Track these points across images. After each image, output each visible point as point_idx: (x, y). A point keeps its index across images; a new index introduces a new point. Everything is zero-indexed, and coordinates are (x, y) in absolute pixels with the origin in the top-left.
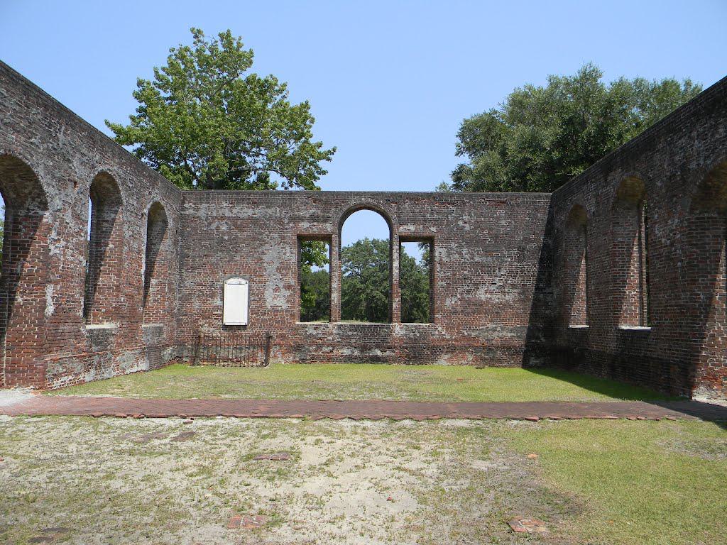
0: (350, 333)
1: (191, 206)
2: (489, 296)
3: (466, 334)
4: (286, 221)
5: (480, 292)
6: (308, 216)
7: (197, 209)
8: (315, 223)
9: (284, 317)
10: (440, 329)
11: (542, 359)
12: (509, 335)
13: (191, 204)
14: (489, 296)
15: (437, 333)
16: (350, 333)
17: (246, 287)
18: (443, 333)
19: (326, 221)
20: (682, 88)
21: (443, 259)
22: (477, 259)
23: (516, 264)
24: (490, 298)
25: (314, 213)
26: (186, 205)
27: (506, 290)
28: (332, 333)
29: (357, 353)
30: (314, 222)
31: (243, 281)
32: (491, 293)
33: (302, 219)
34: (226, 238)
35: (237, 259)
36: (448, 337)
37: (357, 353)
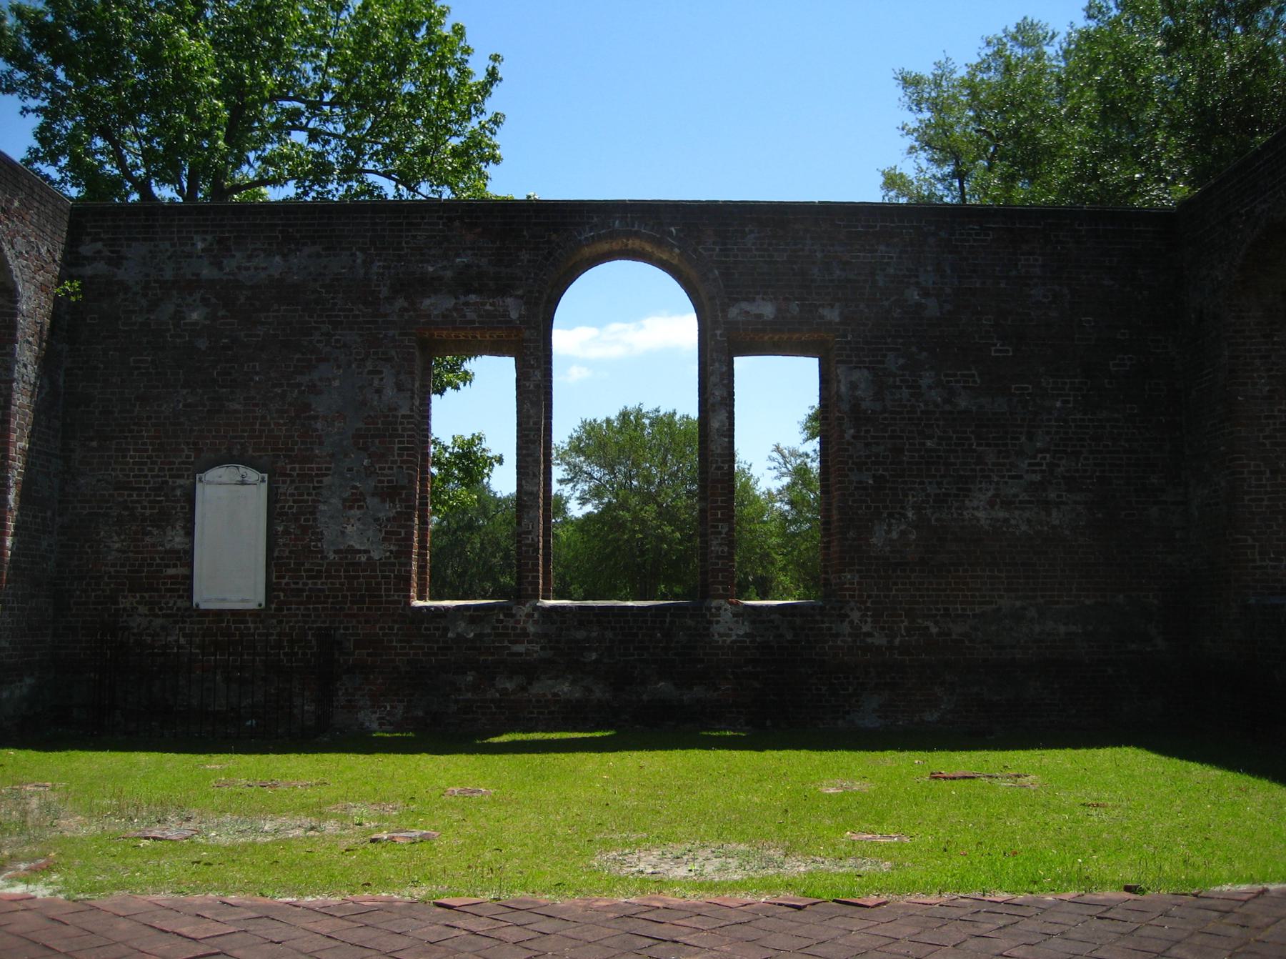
0: (581, 635)
1: (99, 252)
2: (1002, 514)
3: (934, 630)
4: (385, 292)
5: (975, 503)
6: (449, 274)
7: (117, 260)
8: (473, 298)
9: (378, 584)
10: (856, 616)
11: (129, 201)
12: (1062, 629)
13: (99, 245)
14: (1002, 514)
15: (846, 628)
16: (581, 635)
17: (196, 599)
18: (865, 629)
19: (503, 291)
20: (927, 115)
21: (864, 405)
22: (963, 403)
23: (1079, 416)
24: (1006, 520)
25: (468, 266)
26: (86, 249)
27: (1052, 496)
28: (525, 633)
29: (599, 692)
30: (467, 293)
31: (252, 475)
32: (1008, 504)
33: (428, 285)
34: (202, 344)
35: (238, 407)
36: (879, 640)
37: (599, 692)
